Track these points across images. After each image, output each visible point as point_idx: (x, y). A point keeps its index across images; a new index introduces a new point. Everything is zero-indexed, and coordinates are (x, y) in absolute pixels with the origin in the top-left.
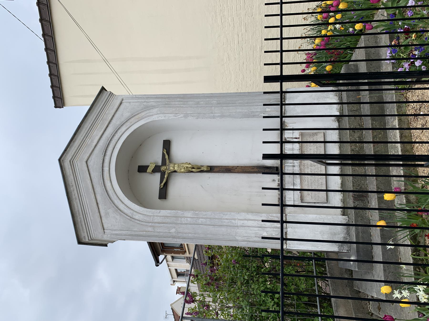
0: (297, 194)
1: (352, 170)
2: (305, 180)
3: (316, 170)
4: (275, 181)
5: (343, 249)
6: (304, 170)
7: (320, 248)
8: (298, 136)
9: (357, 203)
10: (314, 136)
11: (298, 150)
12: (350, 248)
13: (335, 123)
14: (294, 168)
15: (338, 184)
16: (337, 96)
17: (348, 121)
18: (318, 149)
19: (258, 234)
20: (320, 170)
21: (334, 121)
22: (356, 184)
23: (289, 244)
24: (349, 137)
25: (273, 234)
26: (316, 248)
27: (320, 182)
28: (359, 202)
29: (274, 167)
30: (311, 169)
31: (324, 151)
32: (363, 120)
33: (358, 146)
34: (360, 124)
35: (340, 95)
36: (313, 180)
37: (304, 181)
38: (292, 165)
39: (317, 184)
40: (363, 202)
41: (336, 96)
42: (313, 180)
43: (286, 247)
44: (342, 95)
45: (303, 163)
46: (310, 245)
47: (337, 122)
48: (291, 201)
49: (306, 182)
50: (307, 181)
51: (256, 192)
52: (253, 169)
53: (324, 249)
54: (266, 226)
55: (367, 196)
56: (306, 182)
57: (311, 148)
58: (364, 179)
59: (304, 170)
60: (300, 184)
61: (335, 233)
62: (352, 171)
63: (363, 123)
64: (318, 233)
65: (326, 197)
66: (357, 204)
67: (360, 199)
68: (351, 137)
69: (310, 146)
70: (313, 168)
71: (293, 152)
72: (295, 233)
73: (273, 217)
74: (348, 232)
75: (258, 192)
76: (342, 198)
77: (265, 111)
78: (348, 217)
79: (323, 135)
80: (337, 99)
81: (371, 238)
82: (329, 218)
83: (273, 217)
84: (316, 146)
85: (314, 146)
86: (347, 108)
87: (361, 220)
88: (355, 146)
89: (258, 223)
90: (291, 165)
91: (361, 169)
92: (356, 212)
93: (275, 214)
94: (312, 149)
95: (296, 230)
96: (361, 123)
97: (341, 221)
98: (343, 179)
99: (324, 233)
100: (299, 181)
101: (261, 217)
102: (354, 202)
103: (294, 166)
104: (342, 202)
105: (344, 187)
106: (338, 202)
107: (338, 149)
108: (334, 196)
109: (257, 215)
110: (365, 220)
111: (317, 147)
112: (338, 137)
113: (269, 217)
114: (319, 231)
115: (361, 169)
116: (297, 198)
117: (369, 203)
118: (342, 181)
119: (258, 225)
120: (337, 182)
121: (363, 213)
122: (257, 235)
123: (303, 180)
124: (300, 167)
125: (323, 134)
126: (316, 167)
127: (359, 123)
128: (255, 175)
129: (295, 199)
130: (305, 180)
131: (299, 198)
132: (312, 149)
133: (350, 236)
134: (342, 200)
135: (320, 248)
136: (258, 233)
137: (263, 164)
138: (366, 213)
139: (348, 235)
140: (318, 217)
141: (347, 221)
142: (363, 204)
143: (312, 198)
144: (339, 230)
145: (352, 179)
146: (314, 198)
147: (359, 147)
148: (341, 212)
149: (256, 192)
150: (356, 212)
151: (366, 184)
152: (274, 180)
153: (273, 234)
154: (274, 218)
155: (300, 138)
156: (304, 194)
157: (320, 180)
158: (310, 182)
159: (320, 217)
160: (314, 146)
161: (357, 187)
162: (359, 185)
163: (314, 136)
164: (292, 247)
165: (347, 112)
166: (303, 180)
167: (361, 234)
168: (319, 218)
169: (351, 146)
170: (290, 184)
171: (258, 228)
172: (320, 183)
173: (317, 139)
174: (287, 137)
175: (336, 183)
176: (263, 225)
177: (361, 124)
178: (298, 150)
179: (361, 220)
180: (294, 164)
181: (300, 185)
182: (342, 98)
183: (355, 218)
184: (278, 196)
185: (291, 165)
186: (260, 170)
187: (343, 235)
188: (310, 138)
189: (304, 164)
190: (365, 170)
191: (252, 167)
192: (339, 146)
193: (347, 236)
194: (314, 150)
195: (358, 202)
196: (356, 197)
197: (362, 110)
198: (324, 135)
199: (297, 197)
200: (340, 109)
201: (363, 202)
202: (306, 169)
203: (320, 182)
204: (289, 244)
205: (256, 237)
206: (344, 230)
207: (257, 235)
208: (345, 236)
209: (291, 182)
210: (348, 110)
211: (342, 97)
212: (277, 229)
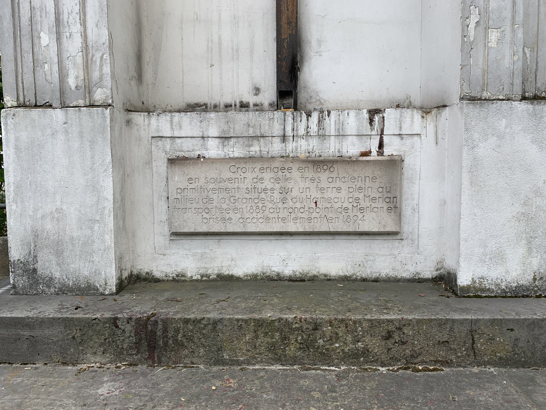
0: (196, 148)
1: (243, 320)
2: (235, 170)
3: (270, 205)
4: (256, 94)
5: (19, 276)
6: (268, 170)
7: (14, 207)
8: (387, 151)
9: (128, 328)
10: (387, 200)
11: (339, 151)
12: (21, 292)
13: (433, 269)
14: (277, 141)
15: (230, 266)
16: (531, 281)
17: (430, 320)
18: (341, 213)
19: (41, 16)
20: (271, 216)
21: (439, 266)
22: (191, 331)
23: (14, 115)
24: (368, 317)
25: (46, 65)
26: (11, 197)
27: (231, 215)
28: (133, 335)
29: (296, 86)
30: (272, 189)
31: (332, 230)
32: (434, 370)
33: (331, 345)
34: (419, 359)
35: (536, 292)
36: (238, 196)
37: (233, 169)
38: (289, 132)
39: (225, 206)
40: (131, 348)
41: (535, 279)
42: (238, 196)
43: (9, 106)
44: (537, 297)
45: (291, 165)
46: (18, 178)
47: (435, 274)
48: (172, 128)
49: (229, 175)
50: (233, 176)
51: (220, 38)
52: (289, 23)
53: (12, 220)
54: (64, 40)
55: (154, 363)
56: (229, 175)
57: (343, 191)
58: (211, 355)
59: (268, 170)
60: (227, 157)
61: (62, 253)
62: (238, 320)
63: (418, 371)
64: (58, 203)
65: (186, 230)
66: (123, 327)
67: (140, 340)
68: (365, 325)
69: (351, 190)
70: (276, 195)
71: (332, 138)
72: (49, 132)
73: (101, 66)
74: (71, 291)
75: (220, 44)
76: (189, 275)
77: (487, 28)
78: (112, 294)
79: (388, 229)
80: (521, 283)
81: (15, 363)
82: (107, 237)
83: (101, 66)
84: (350, 206)
85: (351, 200)
86: (487, 317)
87: (74, 338)
88: (331, 337)
89: (74, 14)
90: (289, 128)
91: (248, 351)
92: (98, 324)
93: (109, 71)
94: (338, 195)
95: (61, 137)
96: (423, 362)
97: (100, 274)
98: (244, 281)
99: (58, 220)
100: (236, 155)
101: (97, 25)
102: (131, 319)
103: (284, 138)
104: (177, 276)
105: (219, 283)
106: (176, 265)
107: (341, 274)
108: (194, 255)
109: (102, 10)
110: (72, 350)
111: (346, 209)
112: (383, 275)
113: (97, 50)
114: (64, 207)
115: (248, 351)
116: (183, 149)
117: (130, 365)
118: (238, 279)
119: (66, 16)
120: (235, 265)
121: (96, 345)
122: (38, 13)
123: (237, 166)
124: (282, 157)
125: (394, 230)
126: (280, 205)
127: (420, 354)
128: (273, 34)
129: (178, 141)
130: (235, 170)
131: (181, 154)
132: (338, 195)
133: (58, 294)
134: (183, 276)
135: (14, 207)
136: (44, 15)
137: (306, 58)
138: (95, 353)
139: (60, 289)
140: (106, 205)
141: (101, 290)
142: (125, 346)
143: (179, 191)
144: (72, 266)
145: (209, 319)
146: (179, 196)
147: (327, 350)
148: (147, 273)
149: (220, 38)
150: (98, 324)
151: (195, 360)
152: (257, 91)
153: (46, 65)
154: (98, 68)
155: (380, 158)
156: (191, 167)
157: (238, 215)
158: (230, 186)
159: (106, 212)
160: (351, 200)
161: (181, 331)
162: (190, 339)
163: (387, 200)
164: (6, 124)
165: (469, 317)
166: (237, 166)
167: (26, 333)
168: (104, 208)
169: (330, 322)
170: (226, 128)
171: (53, 11)
172: (228, 216)
173: (376, 210)
174: (385, 115)
175: (233, 263)
176: (67, 29)
177: (415, 361)
178: (339, 151)
179: (74, 338)
180: (291, 138)
181: (222, 156)
182: (523, 296)
183: (77, 319)
184: (213, 104)
185: (289, 128)
186: (285, 45)
187: (57, 275)
188: (380, 190)
189: (290, 169)
190: (243, 362)
191: (294, 21)
192: (350, 277)
193: (57, 286)
194: (336, 200)
195: (131, 332)
196: (146, 328)
197: (476, 370)
198: (388, 234)
199: (185, 148)
200: (483, 290)
201: (131, 348)
202: (272, 175)
203: (231, 215)
204: (14, 115)
205: (32, 9)
206: (75, 279)
207: (38, 13)
208: (57, 281)
209: (232, 130)
210: (478, 320)
211: (527, 296)
212: (57, 75)
